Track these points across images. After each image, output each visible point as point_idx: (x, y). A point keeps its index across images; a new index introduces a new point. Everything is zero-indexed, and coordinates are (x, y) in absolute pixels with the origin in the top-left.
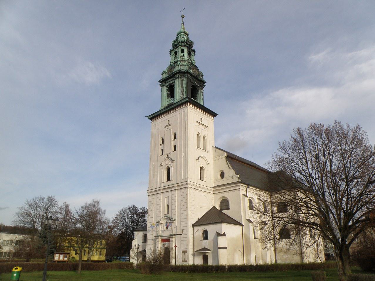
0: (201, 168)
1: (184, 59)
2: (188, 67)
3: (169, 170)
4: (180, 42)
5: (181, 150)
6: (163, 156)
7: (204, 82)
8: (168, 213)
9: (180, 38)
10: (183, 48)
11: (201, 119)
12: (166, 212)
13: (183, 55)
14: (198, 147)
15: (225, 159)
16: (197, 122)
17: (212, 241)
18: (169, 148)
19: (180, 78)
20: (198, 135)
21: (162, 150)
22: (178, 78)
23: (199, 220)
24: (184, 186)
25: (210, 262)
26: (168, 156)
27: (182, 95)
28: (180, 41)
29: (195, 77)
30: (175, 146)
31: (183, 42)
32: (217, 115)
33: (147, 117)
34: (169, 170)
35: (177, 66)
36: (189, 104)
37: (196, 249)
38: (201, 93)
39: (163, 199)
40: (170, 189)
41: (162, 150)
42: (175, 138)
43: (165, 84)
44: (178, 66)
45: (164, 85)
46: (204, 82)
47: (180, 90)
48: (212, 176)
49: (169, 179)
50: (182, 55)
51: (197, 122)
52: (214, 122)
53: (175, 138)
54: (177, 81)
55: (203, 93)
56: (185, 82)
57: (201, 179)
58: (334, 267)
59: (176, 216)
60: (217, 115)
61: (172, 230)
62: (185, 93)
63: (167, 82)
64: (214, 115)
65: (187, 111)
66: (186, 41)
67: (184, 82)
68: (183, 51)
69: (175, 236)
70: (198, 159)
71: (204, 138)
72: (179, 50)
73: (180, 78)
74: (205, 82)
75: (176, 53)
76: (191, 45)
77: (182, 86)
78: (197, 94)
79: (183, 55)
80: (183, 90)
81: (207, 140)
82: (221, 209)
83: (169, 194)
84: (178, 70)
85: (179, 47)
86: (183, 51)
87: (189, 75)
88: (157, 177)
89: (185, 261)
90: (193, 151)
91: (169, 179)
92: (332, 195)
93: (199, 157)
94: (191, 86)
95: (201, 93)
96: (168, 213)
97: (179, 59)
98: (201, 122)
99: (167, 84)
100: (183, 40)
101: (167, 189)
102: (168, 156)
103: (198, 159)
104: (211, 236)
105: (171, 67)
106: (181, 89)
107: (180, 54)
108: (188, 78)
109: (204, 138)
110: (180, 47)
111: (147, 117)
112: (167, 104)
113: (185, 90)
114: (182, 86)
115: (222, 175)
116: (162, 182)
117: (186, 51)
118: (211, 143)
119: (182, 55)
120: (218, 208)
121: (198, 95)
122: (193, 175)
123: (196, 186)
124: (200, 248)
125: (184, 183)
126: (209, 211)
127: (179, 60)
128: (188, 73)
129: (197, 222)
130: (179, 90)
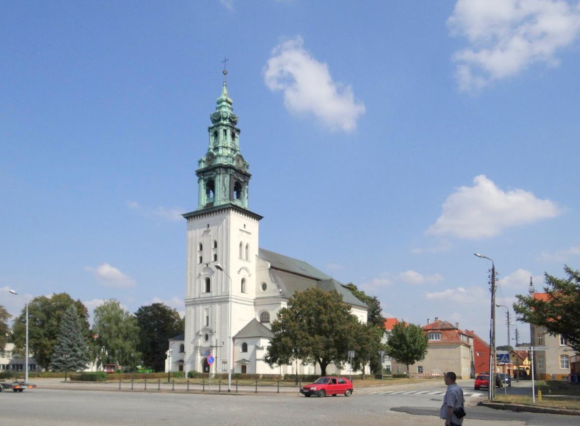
0: (243, 281)
1: (226, 146)
2: (231, 159)
3: (208, 281)
5: (223, 236)
6: (202, 264)
7: (249, 176)
8: (208, 325)
11: (245, 225)
12: (205, 324)
14: (241, 258)
15: (267, 271)
16: (240, 230)
17: (330, 278)
18: (208, 257)
20: (241, 245)
21: (201, 258)
22: (220, 174)
23: (240, 332)
24: (224, 300)
25: (248, 371)
26: (207, 265)
27: (223, 195)
29: (238, 171)
30: (216, 256)
34: (208, 281)
37: (235, 361)
38: (246, 191)
39: (202, 311)
40: (212, 302)
41: (201, 258)
42: (216, 246)
46: (249, 176)
47: (222, 189)
48: (253, 289)
49: (208, 290)
51: (240, 230)
52: (260, 227)
53: (216, 246)
55: (247, 189)
56: (227, 178)
57: (242, 292)
58: (436, 339)
59: (217, 328)
61: (212, 342)
63: (205, 174)
64: (258, 217)
65: (230, 219)
66: (228, 117)
67: (226, 178)
68: (225, 131)
69: (215, 348)
70: (240, 271)
71: (247, 247)
74: (251, 175)
75: (216, 134)
77: (224, 185)
80: (225, 189)
81: (250, 249)
82: (262, 322)
83: (208, 306)
86: (225, 131)
87: (232, 170)
88: (195, 285)
89: (225, 371)
90: (235, 263)
91: (208, 290)
92: (206, 388)
93: (242, 268)
94: (234, 183)
95: (246, 191)
96: (208, 325)
99: (206, 178)
101: (204, 302)
102: (207, 265)
103: (240, 271)
104: (250, 348)
105: (211, 157)
109: (247, 247)
112: (206, 203)
113: (228, 189)
114: (224, 185)
115: (264, 287)
116: (202, 292)
117: (229, 132)
118: (254, 250)
120: (259, 320)
122: (235, 288)
123: (237, 299)
124: (237, 360)
125: (225, 297)
126: (248, 324)
129: (237, 334)
130: (221, 190)
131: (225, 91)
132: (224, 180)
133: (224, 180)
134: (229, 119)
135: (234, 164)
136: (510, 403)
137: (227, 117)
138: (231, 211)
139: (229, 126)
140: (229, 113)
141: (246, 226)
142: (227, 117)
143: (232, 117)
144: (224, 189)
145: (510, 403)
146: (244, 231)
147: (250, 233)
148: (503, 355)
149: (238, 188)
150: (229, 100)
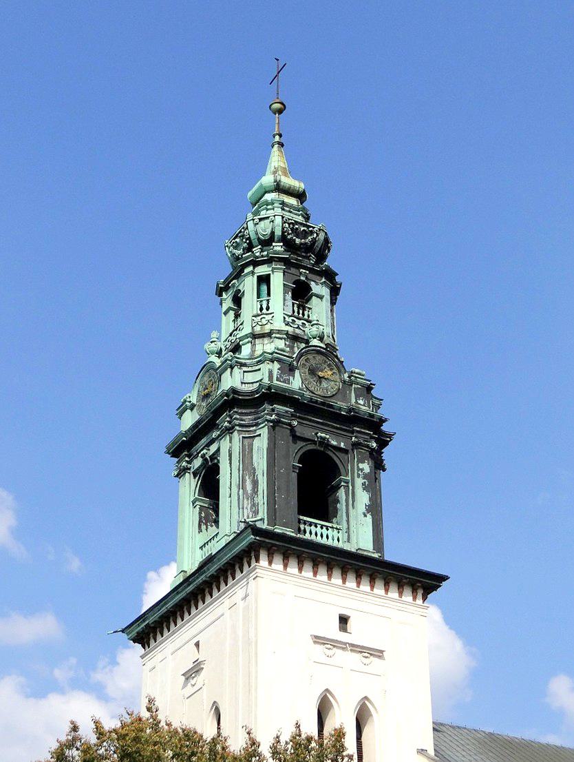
2: (276, 365)
4: (255, 242)
9: (251, 224)
10: (263, 270)
11: (344, 620)
13: (264, 306)
16: (318, 640)
19: (240, 425)
22: (230, 430)
28: (253, 236)
31: (267, 242)
32: (443, 578)
33: (123, 631)
35: (225, 369)
36: (264, 562)
43: (189, 462)
44: (232, 368)
45: (185, 470)
47: (242, 485)
50: (261, 309)
51: (318, 640)
54: (225, 444)
56: (261, 443)
60: (443, 578)
62: (262, 499)
64: (423, 583)
66: (278, 232)
68: (264, 280)
72: (248, 285)
73: (240, 425)
76: (314, 241)
78: (338, 487)
79: (264, 306)
80: (255, 483)
84: (227, 395)
85: (247, 270)
87: (280, 408)
97: (247, 330)
98: (342, 637)
100: (269, 231)
106: (244, 481)
107: (250, 303)
108: (275, 424)
110: (251, 268)
111: (123, 631)
119: (261, 309)
121: (341, 493)
127: (246, 336)
128: (270, 396)
131: (276, 159)
132: (247, 454)
133: (247, 454)
134: (283, 239)
135: (296, 383)
136: (353, 508)
137: (273, 233)
138: (264, 562)
139: (280, 260)
140: (278, 220)
141: (351, 624)
142: (273, 233)
143: (295, 231)
144: (249, 487)
145: (353, 508)
146: (343, 646)
147: (379, 654)
148: (284, 284)
149: (316, 488)
150: (288, 181)
